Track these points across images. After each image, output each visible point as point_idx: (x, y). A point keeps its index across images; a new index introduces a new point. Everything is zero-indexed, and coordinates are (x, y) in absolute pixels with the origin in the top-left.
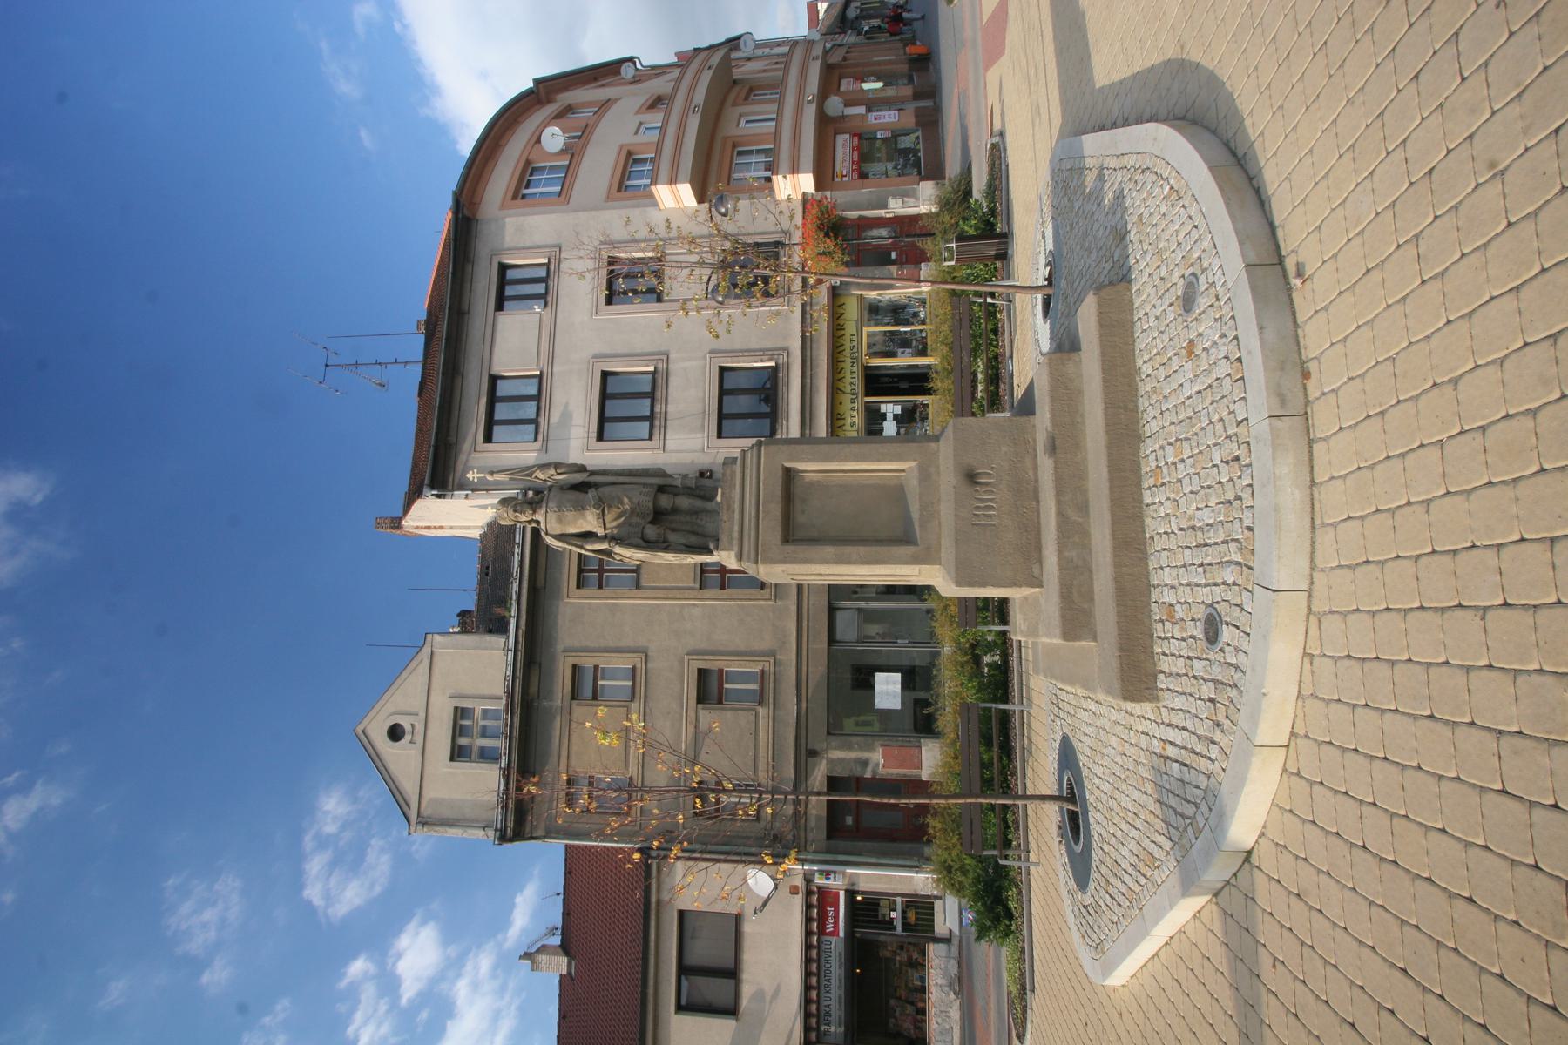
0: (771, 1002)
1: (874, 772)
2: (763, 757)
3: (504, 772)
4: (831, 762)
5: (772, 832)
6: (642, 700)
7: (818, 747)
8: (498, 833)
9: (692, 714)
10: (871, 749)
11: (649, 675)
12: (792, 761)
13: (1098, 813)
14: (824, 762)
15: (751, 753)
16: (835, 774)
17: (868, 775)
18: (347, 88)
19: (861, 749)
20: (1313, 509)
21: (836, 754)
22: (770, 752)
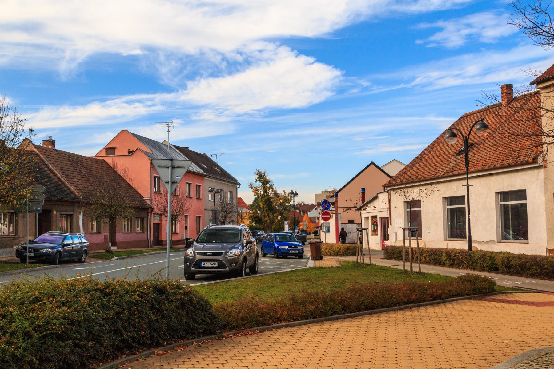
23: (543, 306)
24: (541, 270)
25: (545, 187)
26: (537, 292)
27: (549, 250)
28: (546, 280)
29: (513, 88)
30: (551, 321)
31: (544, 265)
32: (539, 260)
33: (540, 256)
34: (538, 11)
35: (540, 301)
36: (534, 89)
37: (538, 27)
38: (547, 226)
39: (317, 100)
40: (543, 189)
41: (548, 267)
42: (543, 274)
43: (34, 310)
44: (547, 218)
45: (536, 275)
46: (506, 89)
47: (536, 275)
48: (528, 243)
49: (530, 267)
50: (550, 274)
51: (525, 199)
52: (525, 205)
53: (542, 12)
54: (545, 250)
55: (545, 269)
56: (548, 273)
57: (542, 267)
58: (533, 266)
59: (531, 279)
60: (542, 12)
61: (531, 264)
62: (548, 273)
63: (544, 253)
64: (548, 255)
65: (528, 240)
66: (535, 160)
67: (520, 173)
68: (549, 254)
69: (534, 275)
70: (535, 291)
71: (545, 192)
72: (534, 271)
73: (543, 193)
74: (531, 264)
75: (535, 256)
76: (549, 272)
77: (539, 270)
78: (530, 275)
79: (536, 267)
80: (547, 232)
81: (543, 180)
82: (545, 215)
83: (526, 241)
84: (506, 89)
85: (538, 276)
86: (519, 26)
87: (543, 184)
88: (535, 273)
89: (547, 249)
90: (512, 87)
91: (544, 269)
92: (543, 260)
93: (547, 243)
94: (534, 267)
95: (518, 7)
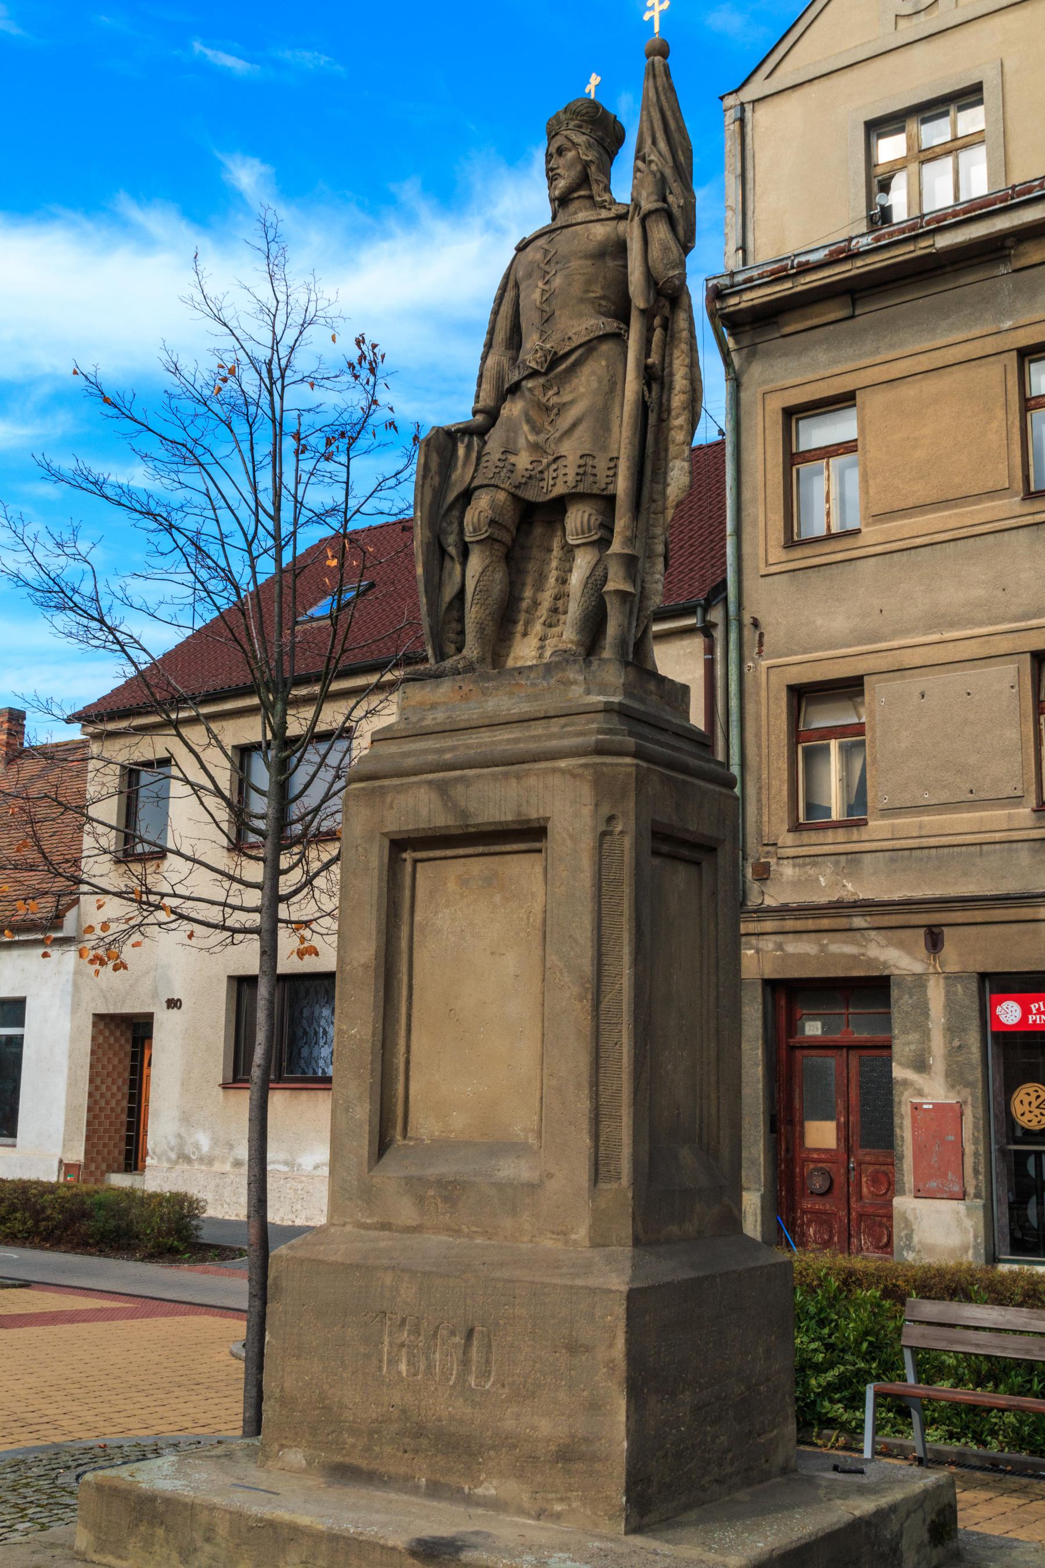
0: (778, 1222)
1: (905, 1083)
2: (921, 826)
3: (842, 251)
4: (920, 981)
5: (773, 861)
6: (1030, 520)
7: (949, 950)
8: (727, 281)
9: (1004, 645)
10: (955, 1077)
11: (835, 570)
12: (918, 894)
13: (363, 714)
14: (918, 968)
15: (927, 798)
16: (895, 993)
17: (899, 1072)
18: (791, 365)
19: (954, 1052)
20: (545, 938)
21: (936, 995)
22: (933, 842)
23: (20, 1327)
24: (36, 1223)
25: (73, 996)
26: (14, 1286)
27: (67, 1165)
28: (46, 1249)
29: (25, 722)
30: (31, 1371)
31: (44, 1209)
32: (35, 1196)
33: (38, 1183)
34: (68, 551)
35: (17, 1312)
36: (75, 733)
37: (63, 592)
38: (67, 1101)
39: (652, 270)
40: (68, 999)
41: (55, 1215)
42: (40, 1233)
43: (921, 859)
44: (69, 1077)
45: (20, 1236)
46: (8, 721)
47: (20, 1236)
48: (14, 1146)
49: (8, 1213)
50: (58, 1232)
51: (21, 1023)
52: (17, 1042)
53: (77, 557)
54: (56, 1165)
55: (48, 1218)
56: (52, 1231)
57: (38, 1213)
58: (15, 1211)
59: (8, 1249)
60: (77, 557)
61: (13, 1205)
62: (52, 1231)
63: (51, 1175)
64: (62, 1180)
65: (15, 1137)
66: (56, 920)
67: (15, 953)
68: (66, 1176)
69: (16, 1237)
70: (10, 1282)
71: (72, 1008)
72: (18, 1226)
73: (69, 1009)
74: (13, 1205)
75: (24, 1182)
76: (56, 1227)
77: (30, 1223)
78: (6, 1236)
79: (23, 1215)
80: (66, 1115)
81: (70, 977)
82: (65, 1070)
83: (9, 1141)
84: (8, 721)
85: (26, 1238)
86: (16, 579)
87: (69, 987)
88: (20, 1232)
89: (61, 1162)
90: (24, 718)
91: (44, 1220)
92: (42, 1194)
93: (64, 1145)
94: (18, 1215)
95: (19, 531)
